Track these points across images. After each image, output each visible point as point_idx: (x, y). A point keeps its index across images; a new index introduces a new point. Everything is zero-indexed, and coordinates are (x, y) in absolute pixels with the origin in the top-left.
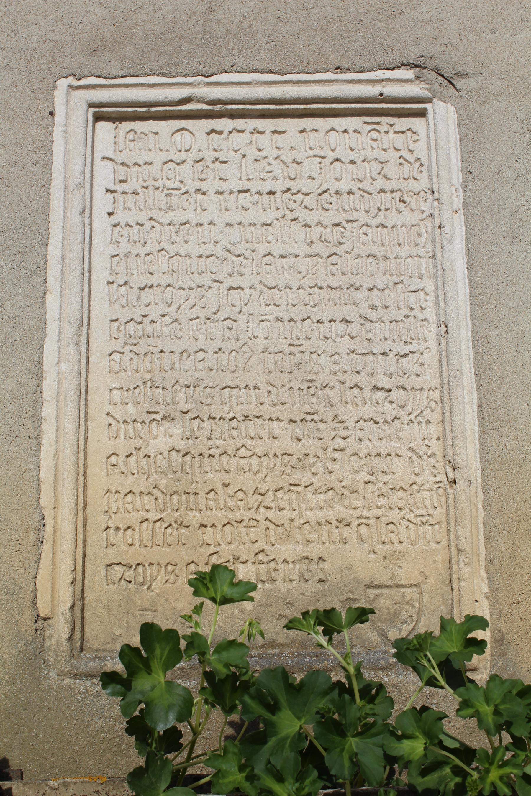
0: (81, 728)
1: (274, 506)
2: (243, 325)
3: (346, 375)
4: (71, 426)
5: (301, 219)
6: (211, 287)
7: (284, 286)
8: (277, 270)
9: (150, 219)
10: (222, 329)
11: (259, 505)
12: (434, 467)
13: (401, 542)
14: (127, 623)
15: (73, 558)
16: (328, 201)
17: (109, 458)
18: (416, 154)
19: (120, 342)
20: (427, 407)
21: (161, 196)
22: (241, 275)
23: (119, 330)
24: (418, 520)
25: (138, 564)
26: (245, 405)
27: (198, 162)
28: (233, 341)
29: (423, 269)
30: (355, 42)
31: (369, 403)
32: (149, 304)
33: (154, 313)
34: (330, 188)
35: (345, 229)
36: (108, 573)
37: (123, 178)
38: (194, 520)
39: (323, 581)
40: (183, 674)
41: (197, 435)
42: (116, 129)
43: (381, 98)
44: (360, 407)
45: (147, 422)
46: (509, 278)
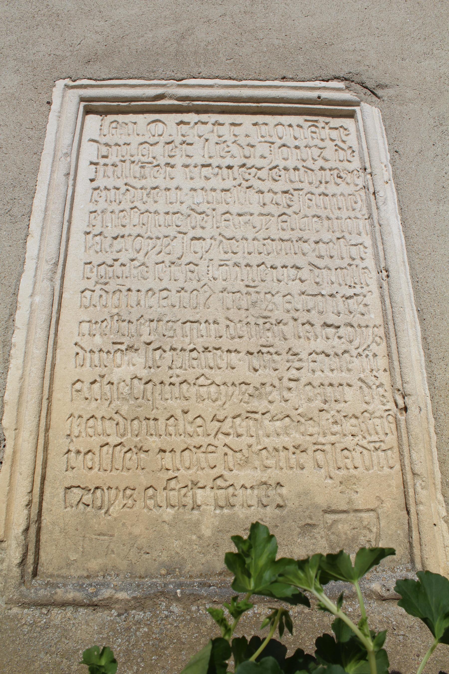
0: (25, 664)
1: (232, 433)
2: (205, 269)
3: (298, 313)
4: (38, 352)
5: (255, 186)
6: (176, 237)
7: (241, 237)
8: (234, 225)
9: (126, 184)
10: (184, 272)
11: (218, 432)
12: (383, 396)
13: (356, 468)
14: (83, 548)
15: (30, 479)
16: (277, 174)
17: (74, 384)
18: (349, 144)
19: (92, 281)
20: (373, 342)
21: (136, 168)
22: (203, 228)
23: (91, 271)
24: (371, 446)
25: (97, 488)
26: (204, 337)
27: (168, 143)
28: (195, 282)
29: (361, 228)
30: (297, 61)
31: (320, 337)
32: (120, 251)
33: (124, 258)
34: (279, 164)
35: (292, 195)
36: (67, 495)
37: (105, 154)
38: (154, 445)
39: (281, 507)
40: (138, 604)
41: (159, 364)
42: (102, 120)
43: (319, 101)
44: (312, 341)
45: (112, 351)
46: (439, 232)
